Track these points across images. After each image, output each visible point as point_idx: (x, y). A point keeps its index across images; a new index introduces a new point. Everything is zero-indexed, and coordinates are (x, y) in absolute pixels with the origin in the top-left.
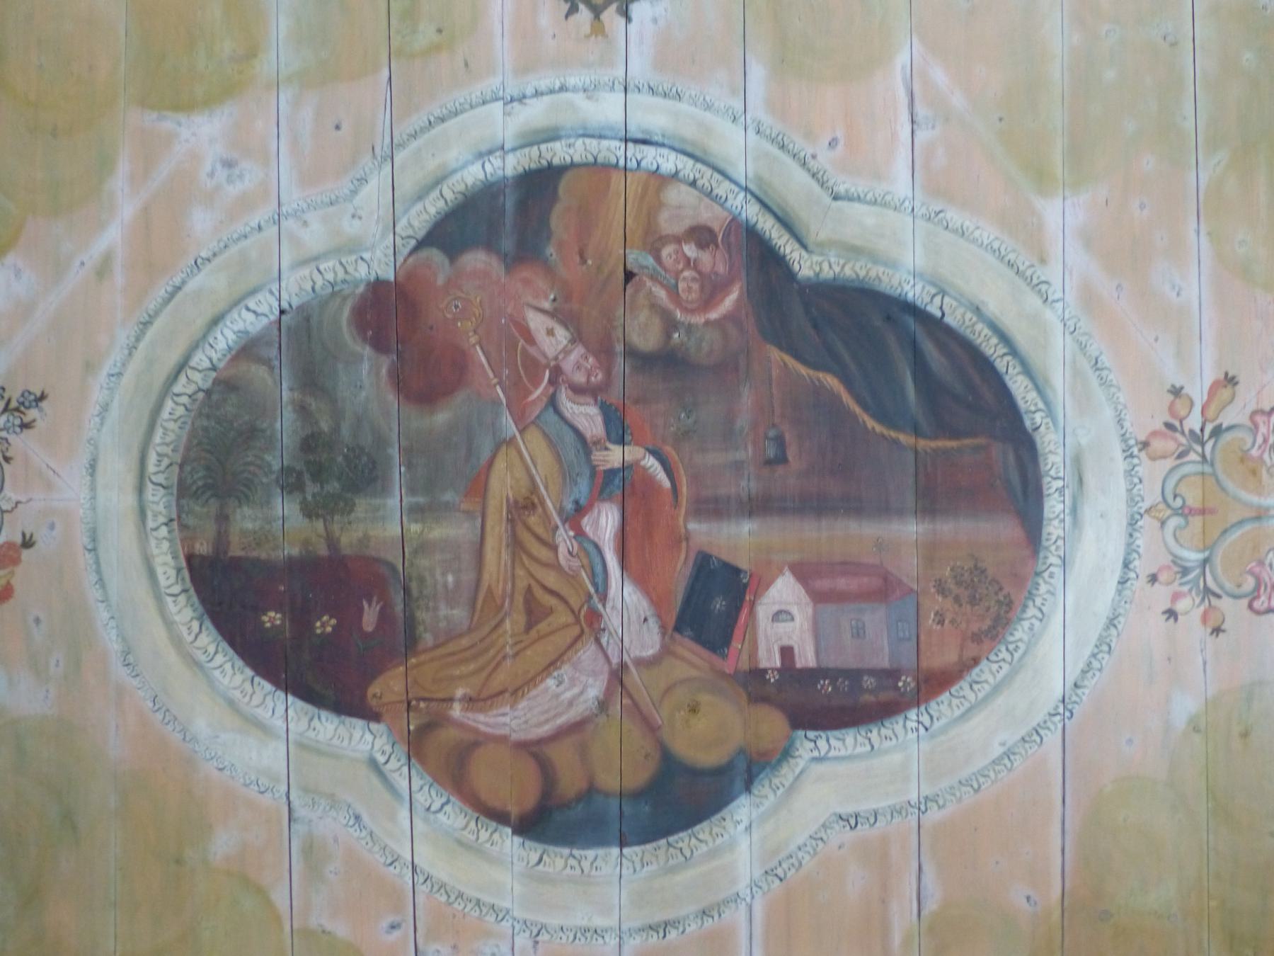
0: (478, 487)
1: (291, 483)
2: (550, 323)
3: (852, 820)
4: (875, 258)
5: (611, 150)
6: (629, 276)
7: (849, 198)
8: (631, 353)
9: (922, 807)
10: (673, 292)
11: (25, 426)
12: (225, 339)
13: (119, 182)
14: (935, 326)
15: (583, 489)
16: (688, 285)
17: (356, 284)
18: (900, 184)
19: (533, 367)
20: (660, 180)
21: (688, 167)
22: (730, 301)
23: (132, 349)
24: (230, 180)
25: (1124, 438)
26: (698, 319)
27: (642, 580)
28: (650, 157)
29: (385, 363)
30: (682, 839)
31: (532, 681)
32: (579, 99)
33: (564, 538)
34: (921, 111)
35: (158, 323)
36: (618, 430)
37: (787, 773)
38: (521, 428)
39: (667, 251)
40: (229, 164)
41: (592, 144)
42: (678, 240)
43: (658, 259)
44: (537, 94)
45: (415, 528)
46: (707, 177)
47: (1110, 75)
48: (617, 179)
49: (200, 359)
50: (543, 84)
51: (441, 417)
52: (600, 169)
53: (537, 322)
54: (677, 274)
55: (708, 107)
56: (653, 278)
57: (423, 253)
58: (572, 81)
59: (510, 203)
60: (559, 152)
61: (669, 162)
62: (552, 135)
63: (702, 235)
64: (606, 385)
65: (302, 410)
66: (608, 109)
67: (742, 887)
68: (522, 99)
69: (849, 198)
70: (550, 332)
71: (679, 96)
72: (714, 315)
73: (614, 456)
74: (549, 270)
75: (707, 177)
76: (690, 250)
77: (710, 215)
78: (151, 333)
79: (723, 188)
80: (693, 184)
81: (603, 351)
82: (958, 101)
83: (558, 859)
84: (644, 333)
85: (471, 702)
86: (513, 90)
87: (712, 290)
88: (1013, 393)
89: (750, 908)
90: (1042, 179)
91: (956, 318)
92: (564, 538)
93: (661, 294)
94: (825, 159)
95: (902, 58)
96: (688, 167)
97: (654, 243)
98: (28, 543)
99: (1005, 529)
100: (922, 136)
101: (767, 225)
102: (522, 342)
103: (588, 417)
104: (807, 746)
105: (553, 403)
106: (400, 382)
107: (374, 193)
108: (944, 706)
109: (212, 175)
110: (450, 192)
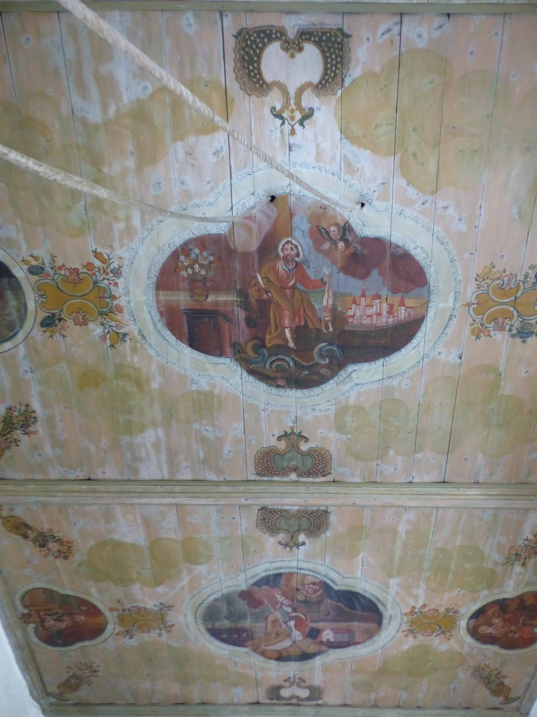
0: (266, 618)
1: (226, 618)
2: (281, 596)
3: (338, 659)
4: (352, 587)
5: (295, 570)
6: (298, 590)
7: (347, 578)
8: (298, 600)
9: (353, 658)
10: (307, 592)
11: (170, 610)
12: (211, 599)
13: (184, 574)
14: (364, 597)
15: (288, 619)
16: (310, 591)
17: (239, 591)
18: (359, 574)
19: (277, 603)
20: (305, 575)
21: (311, 573)
22: (319, 593)
23: (191, 600)
24: (209, 575)
25: (401, 613)
26: (312, 596)
27: (299, 630)
28: (303, 572)
29: (246, 602)
30: (306, 662)
31: (277, 643)
32: (287, 562)
33: (284, 626)
34: (365, 564)
35: (196, 597)
36: (294, 610)
37: (327, 654)
38: (270, 354)
39: (306, 586)
40: (209, 573)
41: (290, 570)
42: (309, 584)
43: (304, 587)
44: (277, 561)
45: (253, 624)
46: (315, 574)
47: (408, 559)
48: (295, 575)
49: (206, 602)
50: (279, 560)
51: (258, 610)
52: (291, 574)
53: (278, 596)
54: (308, 590)
55: (316, 564)
56: (303, 590)
57: (253, 587)
58: (285, 559)
59: (271, 579)
60: (282, 571)
61: (307, 573)
62: (281, 568)
63: (314, 584)
64: (293, 605)
65: (228, 608)
66: (294, 564)
67: (318, 666)
68: (274, 562)
69: (347, 578)
70: (281, 598)
71: (310, 562)
72: (316, 595)
73: (294, 614)
74: (280, 589)
75: (315, 574)
76: (311, 586)
77: (317, 581)
78: (195, 598)
79: (319, 576)
80: (312, 576)
81: (292, 600)
82: (373, 563)
83: (282, 663)
84: (301, 597)
85: (265, 646)
86: (272, 560)
87: (315, 591)
88: (395, 354)
89: (319, 669)
90: (390, 576)
91: (367, 595)
92: (284, 626)
93: (305, 593)
94: (342, 572)
95: (361, 555)
96: (311, 573)
97: (303, 584)
98: (173, 625)
99: (375, 625)
100: (364, 568)
101: (328, 582)
102: (274, 599)
103: (289, 610)
104: (331, 651)
105: (281, 607)
106: (249, 604)
107: (242, 577)
108: (359, 646)
109: (205, 574)
110: (258, 578)
